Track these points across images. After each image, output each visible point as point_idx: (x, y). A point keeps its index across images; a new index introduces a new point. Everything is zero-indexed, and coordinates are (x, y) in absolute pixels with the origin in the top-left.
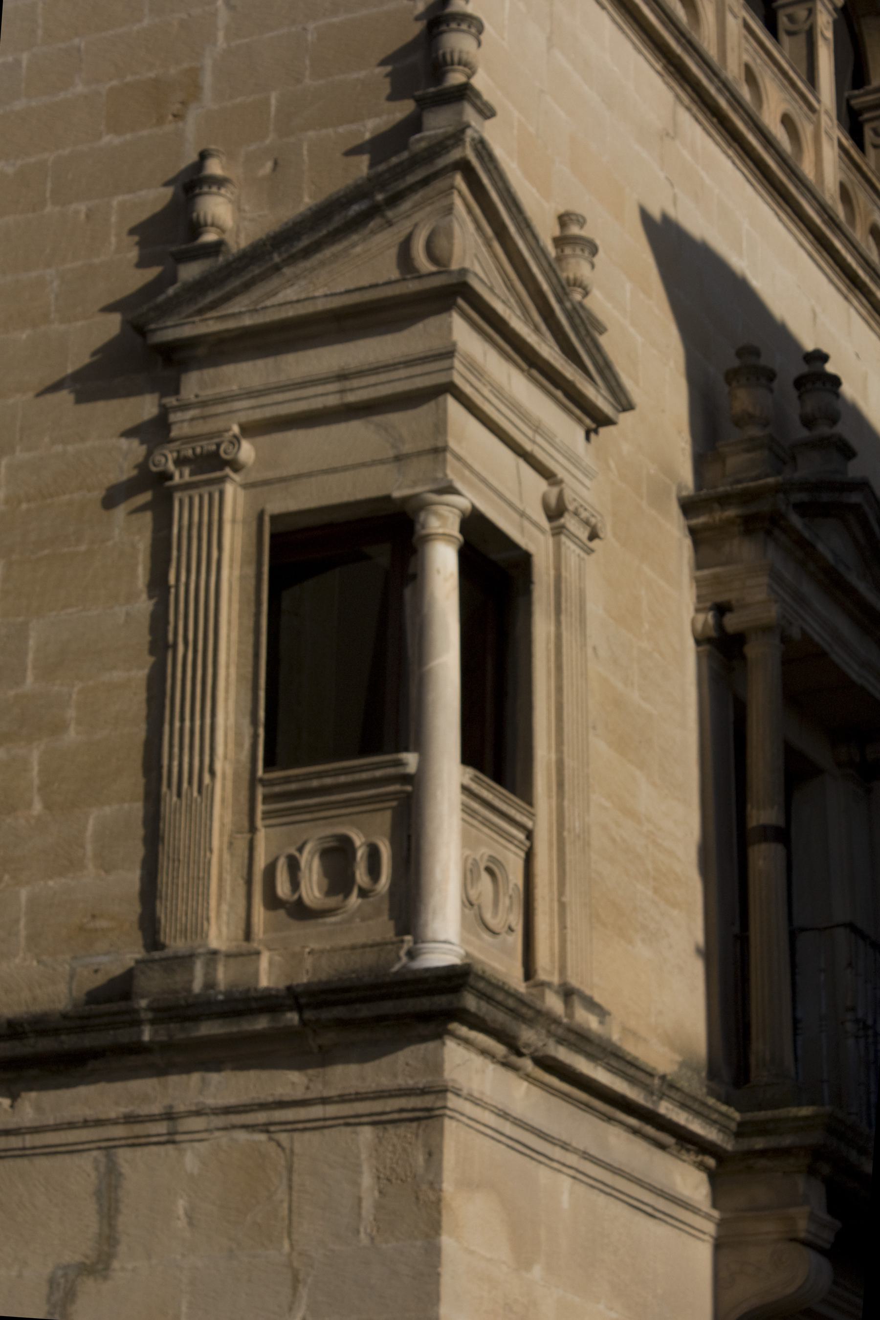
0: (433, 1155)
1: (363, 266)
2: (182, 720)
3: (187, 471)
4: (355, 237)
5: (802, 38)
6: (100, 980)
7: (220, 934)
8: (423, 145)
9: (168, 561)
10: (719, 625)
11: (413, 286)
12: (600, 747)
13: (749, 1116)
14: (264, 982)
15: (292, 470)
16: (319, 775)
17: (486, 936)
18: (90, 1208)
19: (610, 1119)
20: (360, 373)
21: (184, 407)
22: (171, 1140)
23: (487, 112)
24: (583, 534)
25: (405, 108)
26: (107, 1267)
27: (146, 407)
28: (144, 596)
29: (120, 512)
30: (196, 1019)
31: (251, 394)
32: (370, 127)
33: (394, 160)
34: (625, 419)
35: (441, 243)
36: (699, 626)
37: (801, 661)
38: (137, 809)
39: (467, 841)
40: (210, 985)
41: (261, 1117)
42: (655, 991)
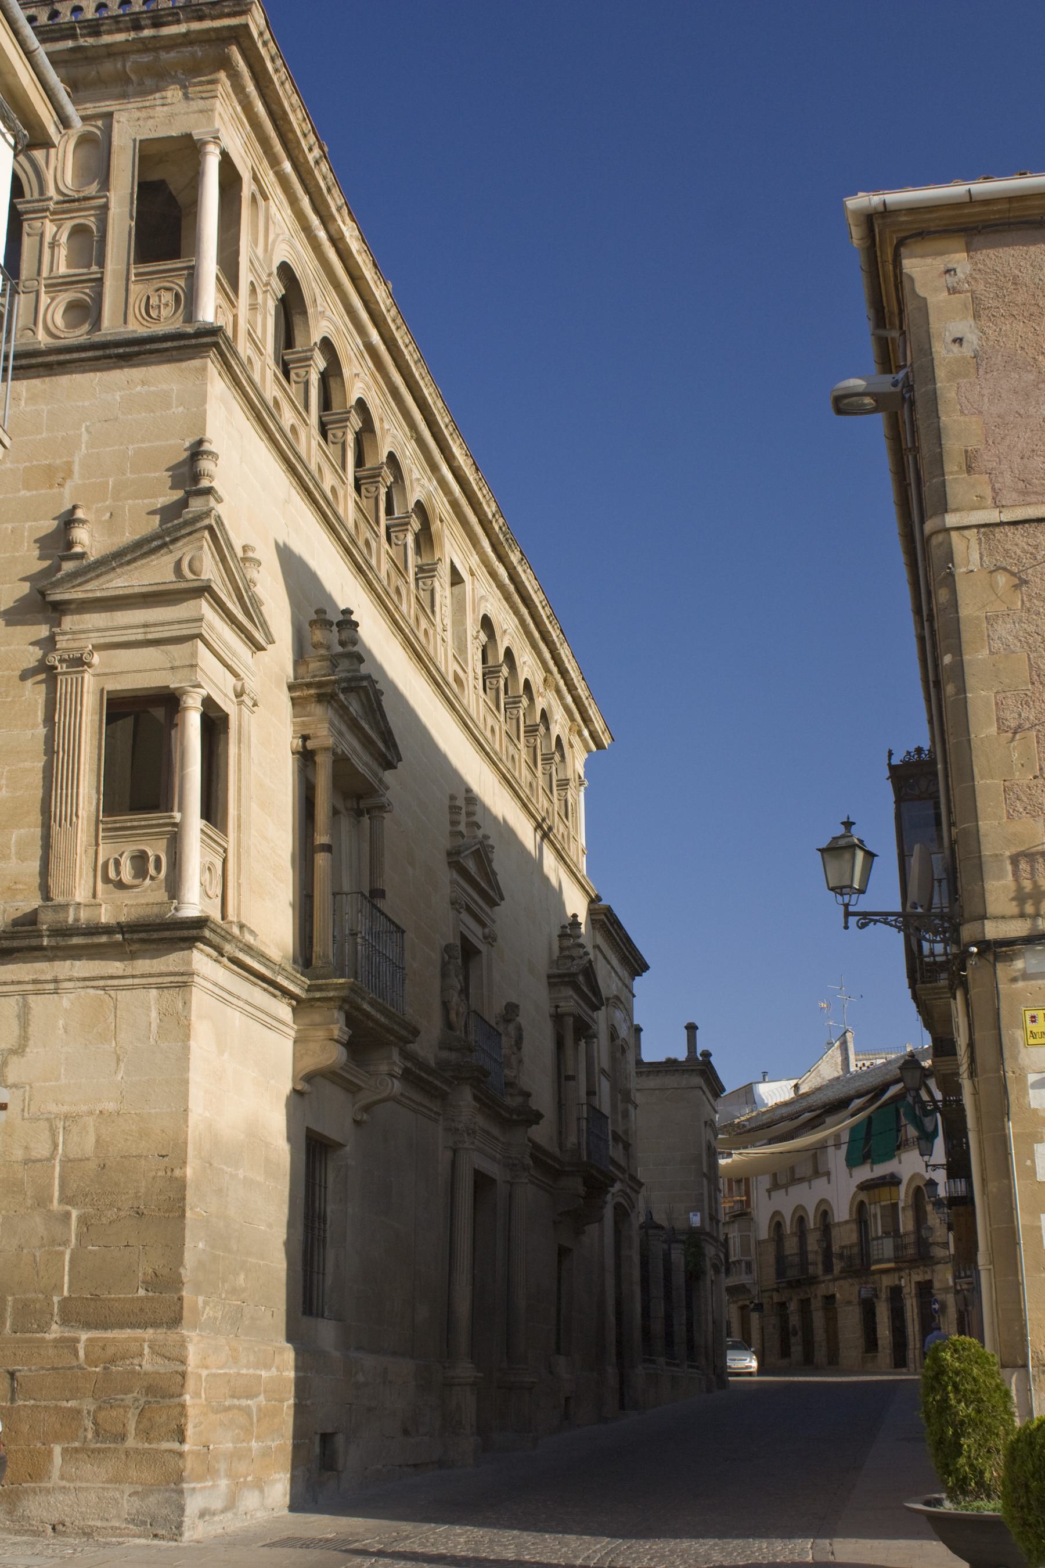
0: (186, 1003)
1: (156, 572)
2: (62, 789)
3: (64, 666)
4: (154, 557)
5: (339, 446)
6: (19, 914)
7: (81, 895)
8: (191, 516)
9: (55, 710)
10: (304, 746)
11: (184, 585)
12: (255, 807)
13: (314, 982)
14: (103, 920)
15: (119, 670)
16: (131, 820)
17: (207, 899)
18: (15, 1024)
19: (255, 984)
20: (155, 625)
21: (64, 634)
22: (56, 992)
23: (219, 500)
24: (250, 703)
25: (178, 494)
26: (23, 1051)
27: (43, 631)
28: (42, 726)
29: (29, 683)
30: (71, 935)
31: (98, 630)
32: (161, 501)
33: (176, 522)
34: (269, 647)
35: (196, 564)
36: (294, 746)
37: (340, 761)
38: (38, 831)
39: (202, 856)
40: (77, 920)
41: (102, 983)
42: (270, 920)
